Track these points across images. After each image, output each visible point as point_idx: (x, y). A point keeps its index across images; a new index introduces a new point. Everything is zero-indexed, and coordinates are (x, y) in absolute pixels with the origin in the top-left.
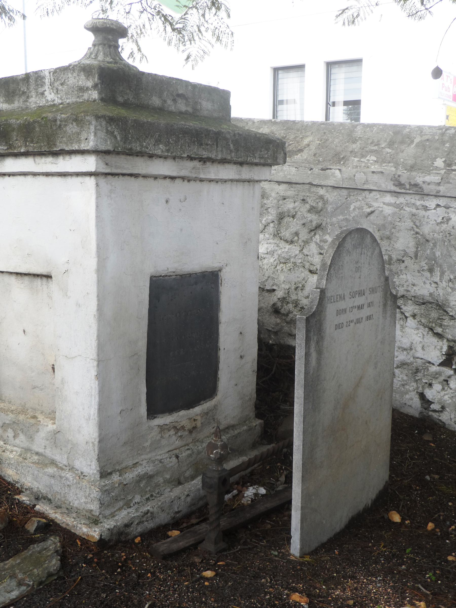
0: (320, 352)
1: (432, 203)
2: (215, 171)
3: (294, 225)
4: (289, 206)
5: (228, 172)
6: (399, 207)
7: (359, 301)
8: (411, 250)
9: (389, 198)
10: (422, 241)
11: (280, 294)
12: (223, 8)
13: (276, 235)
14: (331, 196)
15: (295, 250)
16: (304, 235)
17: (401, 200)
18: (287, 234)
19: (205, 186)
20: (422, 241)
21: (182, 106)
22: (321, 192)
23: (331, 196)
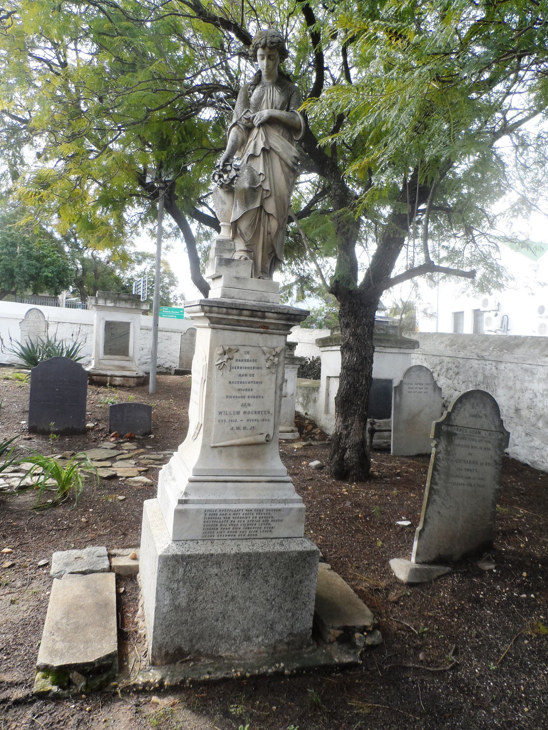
0: (401, 398)
1: (487, 363)
2: (388, 350)
3: (451, 373)
4: (450, 365)
5: (396, 350)
6: (479, 364)
7: (421, 386)
8: (482, 381)
9: (476, 362)
10: (485, 377)
11: (445, 399)
12: (239, 347)
13: (446, 377)
14: (461, 361)
15: (451, 382)
16: (454, 376)
17: (480, 362)
18: (449, 376)
19: (387, 354)
20: (485, 377)
21: (382, 332)
22: (459, 360)
23: (461, 361)
